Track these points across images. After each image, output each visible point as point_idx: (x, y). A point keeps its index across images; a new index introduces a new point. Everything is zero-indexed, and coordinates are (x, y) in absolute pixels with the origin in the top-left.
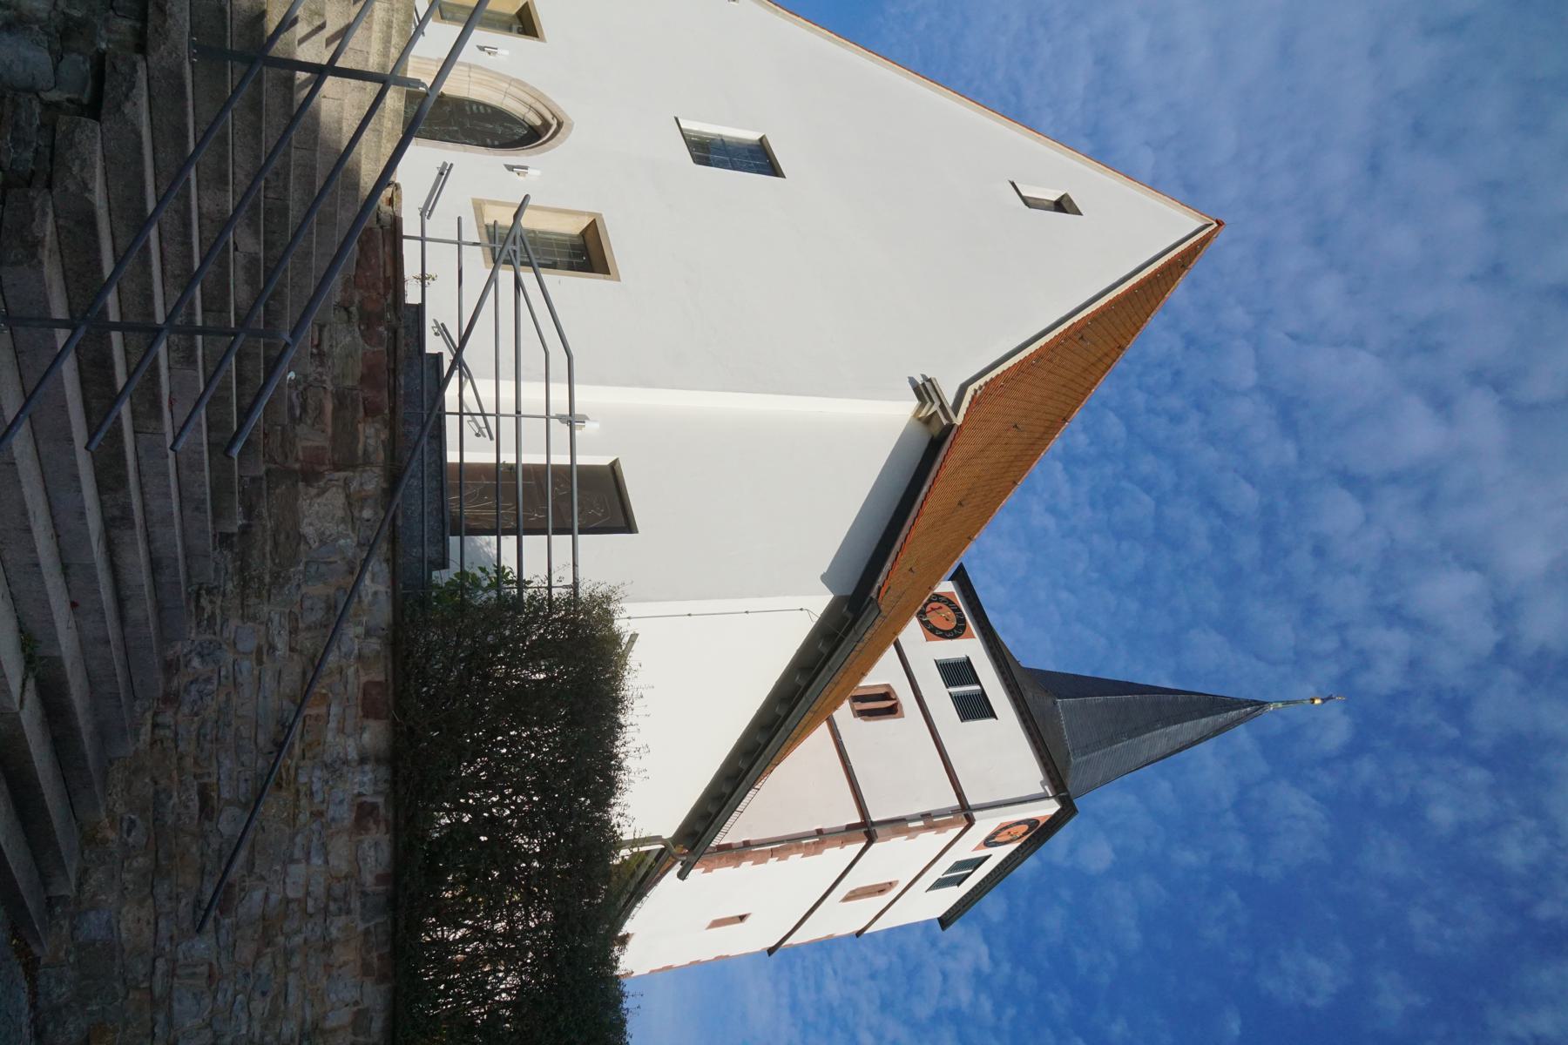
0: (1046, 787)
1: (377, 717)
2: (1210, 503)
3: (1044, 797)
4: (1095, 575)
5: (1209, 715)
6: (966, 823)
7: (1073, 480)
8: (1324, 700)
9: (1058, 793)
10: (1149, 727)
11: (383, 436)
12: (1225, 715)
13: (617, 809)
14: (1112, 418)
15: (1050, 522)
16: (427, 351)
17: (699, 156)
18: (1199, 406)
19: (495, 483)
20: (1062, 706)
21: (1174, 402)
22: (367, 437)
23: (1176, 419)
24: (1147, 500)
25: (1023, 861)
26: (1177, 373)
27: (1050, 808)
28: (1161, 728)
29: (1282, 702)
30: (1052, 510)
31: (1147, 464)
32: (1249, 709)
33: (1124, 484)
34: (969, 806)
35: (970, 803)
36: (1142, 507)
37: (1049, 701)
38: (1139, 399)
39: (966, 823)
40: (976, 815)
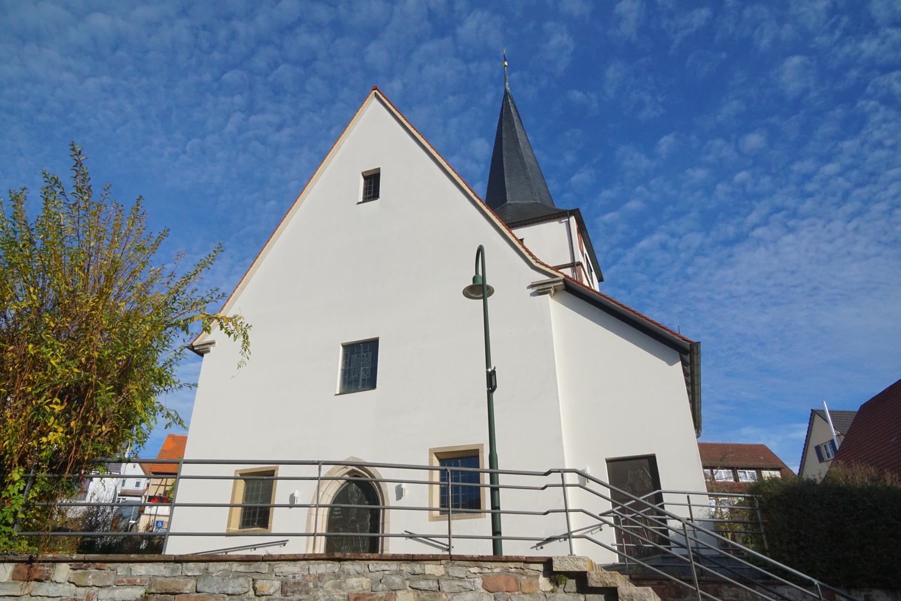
0: (563, 221)
1: (334, 554)
2: (287, 29)
3: (568, 224)
4: (324, 111)
5: (514, 123)
6: (580, 266)
7: (263, 110)
8: (505, 60)
9: (567, 215)
10: (521, 157)
11: (726, 588)
12: (513, 114)
13: (817, 477)
14: (226, 76)
15: (287, 131)
16: (574, 581)
17: (748, 497)
18: (228, 18)
19: (134, 507)
20: (511, 201)
21: (222, 34)
22: (729, 595)
23: (234, 35)
24: (283, 68)
25: (589, 238)
26: (205, 27)
27: (573, 220)
28: (521, 150)
29: (505, 83)
30: (279, 128)
31: (260, 62)
32: (509, 101)
33: (270, 79)
34: (572, 263)
35: (570, 262)
36: (286, 73)
37: (509, 207)
38: (216, 56)
39: (580, 266)
40: (576, 260)
